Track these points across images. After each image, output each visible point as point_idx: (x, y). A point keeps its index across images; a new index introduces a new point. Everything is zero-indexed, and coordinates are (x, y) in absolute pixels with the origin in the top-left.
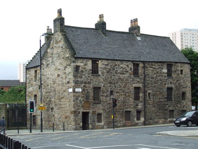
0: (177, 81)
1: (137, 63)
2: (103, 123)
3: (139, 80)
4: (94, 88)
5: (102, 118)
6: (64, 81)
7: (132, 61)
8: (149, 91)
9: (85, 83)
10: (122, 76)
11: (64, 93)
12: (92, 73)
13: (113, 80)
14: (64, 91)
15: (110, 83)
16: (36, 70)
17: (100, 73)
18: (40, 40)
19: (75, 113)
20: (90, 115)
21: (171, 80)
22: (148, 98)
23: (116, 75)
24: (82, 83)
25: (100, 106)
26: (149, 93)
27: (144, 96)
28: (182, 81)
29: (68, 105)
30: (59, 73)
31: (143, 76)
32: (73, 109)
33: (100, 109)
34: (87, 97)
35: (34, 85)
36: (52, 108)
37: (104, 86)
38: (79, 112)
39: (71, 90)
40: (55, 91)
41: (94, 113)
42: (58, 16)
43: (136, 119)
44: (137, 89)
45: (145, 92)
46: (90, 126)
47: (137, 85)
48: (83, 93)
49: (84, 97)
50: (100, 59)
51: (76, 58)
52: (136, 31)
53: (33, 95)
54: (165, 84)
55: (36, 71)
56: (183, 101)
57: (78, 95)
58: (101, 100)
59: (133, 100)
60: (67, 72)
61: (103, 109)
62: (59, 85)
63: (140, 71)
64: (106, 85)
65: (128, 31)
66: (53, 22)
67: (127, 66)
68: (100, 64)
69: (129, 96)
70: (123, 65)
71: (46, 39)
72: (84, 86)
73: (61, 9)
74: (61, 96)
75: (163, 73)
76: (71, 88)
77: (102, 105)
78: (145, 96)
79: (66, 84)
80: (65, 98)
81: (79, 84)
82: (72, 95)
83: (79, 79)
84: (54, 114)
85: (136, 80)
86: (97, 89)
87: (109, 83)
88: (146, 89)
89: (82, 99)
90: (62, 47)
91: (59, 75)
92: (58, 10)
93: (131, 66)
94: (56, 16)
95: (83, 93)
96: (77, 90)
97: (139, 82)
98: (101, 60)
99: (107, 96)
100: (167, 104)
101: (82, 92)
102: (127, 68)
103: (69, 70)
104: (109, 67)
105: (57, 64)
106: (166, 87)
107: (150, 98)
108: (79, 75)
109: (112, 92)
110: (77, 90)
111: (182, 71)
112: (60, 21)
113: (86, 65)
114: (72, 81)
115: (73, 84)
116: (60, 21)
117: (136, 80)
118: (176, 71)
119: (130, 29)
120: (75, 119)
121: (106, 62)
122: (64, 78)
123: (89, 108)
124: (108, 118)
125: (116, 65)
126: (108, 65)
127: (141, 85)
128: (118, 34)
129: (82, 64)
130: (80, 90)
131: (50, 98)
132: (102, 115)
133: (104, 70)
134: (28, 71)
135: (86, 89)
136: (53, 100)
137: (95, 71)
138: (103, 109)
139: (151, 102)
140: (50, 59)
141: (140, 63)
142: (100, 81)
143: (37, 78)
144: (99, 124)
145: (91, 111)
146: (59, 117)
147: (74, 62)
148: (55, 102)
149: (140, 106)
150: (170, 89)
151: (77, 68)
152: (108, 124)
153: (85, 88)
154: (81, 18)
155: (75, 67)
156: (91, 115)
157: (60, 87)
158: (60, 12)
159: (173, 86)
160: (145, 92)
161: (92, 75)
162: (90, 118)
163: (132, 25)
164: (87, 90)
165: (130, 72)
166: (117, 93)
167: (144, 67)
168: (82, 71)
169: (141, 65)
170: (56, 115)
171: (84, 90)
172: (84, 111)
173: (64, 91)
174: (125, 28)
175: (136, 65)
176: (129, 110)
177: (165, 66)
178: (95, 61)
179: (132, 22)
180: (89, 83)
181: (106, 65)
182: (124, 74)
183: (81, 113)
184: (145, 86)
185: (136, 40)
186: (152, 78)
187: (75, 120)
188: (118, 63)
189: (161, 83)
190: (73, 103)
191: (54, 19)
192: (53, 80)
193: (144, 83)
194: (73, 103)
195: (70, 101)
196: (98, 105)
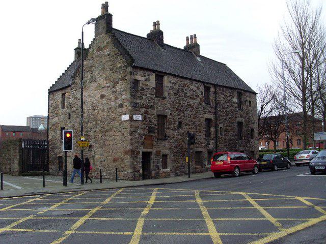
0: (247, 114)
1: (208, 85)
2: (168, 170)
3: (210, 109)
4: (159, 116)
5: (169, 161)
6: (113, 103)
7: (203, 82)
8: (221, 125)
9: (147, 107)
11: (113, 122)
12: (156, 94)
13: (182, 106)
14: (113, 120)
15: (178, 110)
16: (63, 92)
17: (166, 94)
18: (83, 32)
19: (133, 153)
20: (153, 156)
21: (241, 113)
22: (219, 135)
23: (185, 99)
24: (142, 106)
25: (166, 144)
27: (216, 130)
28: (250, 115)
30: (103, 93)
31: (214, 104)
32: (129, 148)
33: (165, 148)
34: (150, 130)
35: (60, 114)
37: (171, 114)
38: (138, 152)
39: (126, 117)
40: (95, 119)
41: (158, 153)
42: (103, 12)
43: (206, 163)
46: (153, 173)
48: (144, 122)
49: (145, 129)
50: (166, 74)
53: (59, 128)
54: (236, 118)
55: (64, 95)
56: (252, 140)
57: (137, 124)
58: (168, 135)
59: (204, 137)
60: (118, 90)
61: (170, 149)
62: (103, 111)
63: (212, 97)
64: (173, 113)
67: (198, 89)
68: (167, 81)
69: (200, 131)
70: (193, 87)
71: (77, 55)
72: (146, 112)
73: (107, 3)
74: (107, 128)
75: (234, 103)
76: (126, 114)
77: (168, 142)
78: (216, 131)
79: (115, 108)
80: (114, 129)
81: (138, 109)
82: (127, 125)
83: (138, 101)
84: (94, 154)
85: (207, 109)
86: (162, 117)
88: (218, 122)
90: (109, 55)
91: (103, 96)
92: (103, 5)
94: (98, 13)
95: (144, 122)
97: (210, 112)
98: (168, 76)
99: (174, 129)
100: (237, 144)
101: (143, 120)
102: (198, 91)
104: (177, 87)
105: (102, 81)
106: (237, 121)
108: (139, 94)
109: (180, 123)
110: (135, 117)
111: (250, 102)
112: (104, 21)
113: (147, 80)
115: (128, 106)
116: (104, 21)
117: (207, 109)
118: (245, 101)
119: (185, 47)
120: (133, 163)
121: (173, 80)
122: (113, 99)
123: (152, 146)
124: (175, 161)
125: (185, 85)
126: (175, 84)
127: (212, 117)
129: (142, 79)
130: (140, 118)
131: (87, 131)
132: (168, 156)
133: (171, 91)
134: (51, 96)
135: (147, 116)
136: (92, 133)
137: (159, 91)
138: (170, 149)
141: (211, 86)
142: (165, 106)
143: (66, 104)
144: (164, 170)
146: (103, 160)
148: (95, 137)
149: (211, 146)
150: (240, 124)
152: (176, 170)
153: (146, 115)
154: (132, 22)
155: (133, 81)
156: (155, 156)
157: (106, 114)
158: (105, 7)
159: (243, 120)
161: (156, 97)
162: (152, 161)
163: (188, 43)
164: (149, 118)
165: (201, 97)
166: (186, 125)
167: (215, 93)
168: (143, 89)
169: (212, 89)
170: (97, 157)
171: (144, 118)
172: (145, 150)
173: (113, 120)
174: (181, 45)
175: (207, 89)
176: (199, 149)
177: (236, 94)
178: (160, 76)
179: (187, 39)
180: (152, 108)
181: (173, 83)
182: (194, 99)
183: (141, 153)
184: (216, 119)
185: (196, 60)
186: (224, 108)
188: (187, 82)
189: (232, 115)
190: (130, 137)
191: (52, 79)
192: (93, 103)
193: (215, 114)
194: (130, 137)
195: (124, 134)
196: (164, 142)
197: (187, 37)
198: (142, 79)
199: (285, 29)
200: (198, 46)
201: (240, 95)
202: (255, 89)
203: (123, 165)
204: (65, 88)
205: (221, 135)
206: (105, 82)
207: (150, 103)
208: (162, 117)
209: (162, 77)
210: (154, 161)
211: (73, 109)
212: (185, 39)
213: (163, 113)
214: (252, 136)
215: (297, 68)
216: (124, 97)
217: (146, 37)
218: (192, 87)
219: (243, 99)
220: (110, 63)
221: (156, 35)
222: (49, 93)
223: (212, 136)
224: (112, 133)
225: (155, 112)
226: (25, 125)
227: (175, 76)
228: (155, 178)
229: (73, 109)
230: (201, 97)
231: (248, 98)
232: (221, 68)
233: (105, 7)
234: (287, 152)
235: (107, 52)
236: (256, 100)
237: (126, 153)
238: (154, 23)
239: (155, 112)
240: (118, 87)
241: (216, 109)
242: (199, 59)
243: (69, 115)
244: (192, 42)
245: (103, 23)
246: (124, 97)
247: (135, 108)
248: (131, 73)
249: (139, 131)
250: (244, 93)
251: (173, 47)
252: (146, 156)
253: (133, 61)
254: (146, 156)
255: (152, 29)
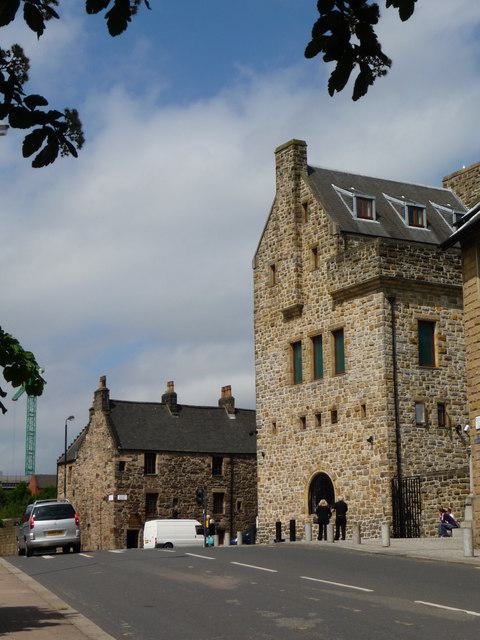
7: (211, 454)
9: (134, 487)
10: (193, 477)
12: (145, 472)
13: (179, 482)
15: (174, 487)
17: (157, 472)
19: (115, 531)
26: (239, 503)
29: (108, 520)
36: (89, 525)
39: (111, 498)
44: (218, 497)
45: (231, 501)
47: (218, 490)
55: (70, 468)
65: (217, 405)
78: (232, 507)
82: (112, 504)
83: (124, 482)
87: (172, 487)
88: (235, 496)
89: (128, 511)
91: (97, 475)
93: (209, 460)
94: (98, 386)
96: (119, 497)
103: (110, 468)
110: (119, 497)
114: (113, 485)
125: (184, 460)
127: (225, 490)
128: (205, 411)
130: (125, 497)
137: (149, 468)
139: (241, 516)
140: (88, 450)
147: (116, 456)
151: (121, 465)
158: (103, 381)
160: (231, 501)
163: (223, 395)
167: (231, 463)
170: (93, 535)
171: (131, 497)
178: (150, 457)
180: (140, 487)
184: (232, 492)
186: (245, 479)
213: (154, 492)
222: (59, 464)
227: (169, 452)
234: (423, 421)
247: (120, 488)
251: (200, 408)
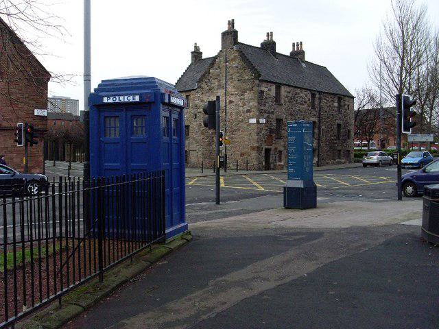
2: (282, 163)
4: (277, 119)
5: (283, 156)
6: (241, 109)
8: (323, 127)
9: (269, 113)
10: (301, 107)
14: (242, 122)
15: (291, 115)
16: (188, 94)
17: (282, 102)
19: (259, 149)
20: (272, 152)
30: (231, 99)
32: (256, 145)
33: (280, 144)
34: (271, 131)
39: (253, 121)
46: (272, 166)
51: (260, 81)
52: (300, 56)
55: (187, 96)
57: (262, 126)
63: (317, 102)
66: (48, 69)
68: (283, 90)
72: (268, 117)
76: (253, 118)
86: (279, 121)
94: (225, 28)
107: (323, 135)
115: (255, 111)
119: (291, 53)
121: (288, 89)
127: (316, 119)
129: (266, 90)
142: (281, 112)
145: (273, 149)
150: (339, 125)
154: (251, 37)
158: (231, 23)
159: (341, 122)
162: (271, 156)
163: (294, 48)
167: (320, 98)
169: (317, 96)
171: (267, 121)
173: (242, 122)
175: (313, 96)
178: (278, 86)
180: (273, 113)
182: (303, 104)
184: (319, 121)
187: (258, 158)
188: (298, 91)
194: (257, 137)
197: (294, 44)
198: (266, 90)
199: (387, 26)
200: (304, 52)
201: (340, 99)
202: (353, 93)
203: (249, 158)
204: (190, 91)
205: (323, 135)
206: (233, 90)
207: (271, 109)
208: (279, 121)
209: (280, 87)
210: (273, 155)
211: (199, 110)
212: (266, 35)
214: (349, 137)
215: (396, 69)
216: (251, 104)
217: (259, 46)
218: (301, 94)
219: (342, 103)
220: (237, 75)
221: (269, 46)
223: (316, 136)
224: (240, 133)
225: (274, 116)
226: (50, 96)
228: (273, 169)
229: (199, 110)
230: (308, 102)
231: (346, 103)
232: (322, 72)
233: (231, 23)
235: (235, 64)
236: (354, 103)
237: (253, 149)
238: (268, 34)
239: (274, 116)
240: (247, 96)
241: (320, 114)
242: (304, 65)
243: (196, 115)
244: (298, 48)
245: (230, 38)
246: (251, 104)
247: (261, 113)
248: (259, 86)
249: (263, 132)
250: (343, 97)
252: (268, 151)
253: (260, 75)
254: (268, 151)
255: (266, 38)
